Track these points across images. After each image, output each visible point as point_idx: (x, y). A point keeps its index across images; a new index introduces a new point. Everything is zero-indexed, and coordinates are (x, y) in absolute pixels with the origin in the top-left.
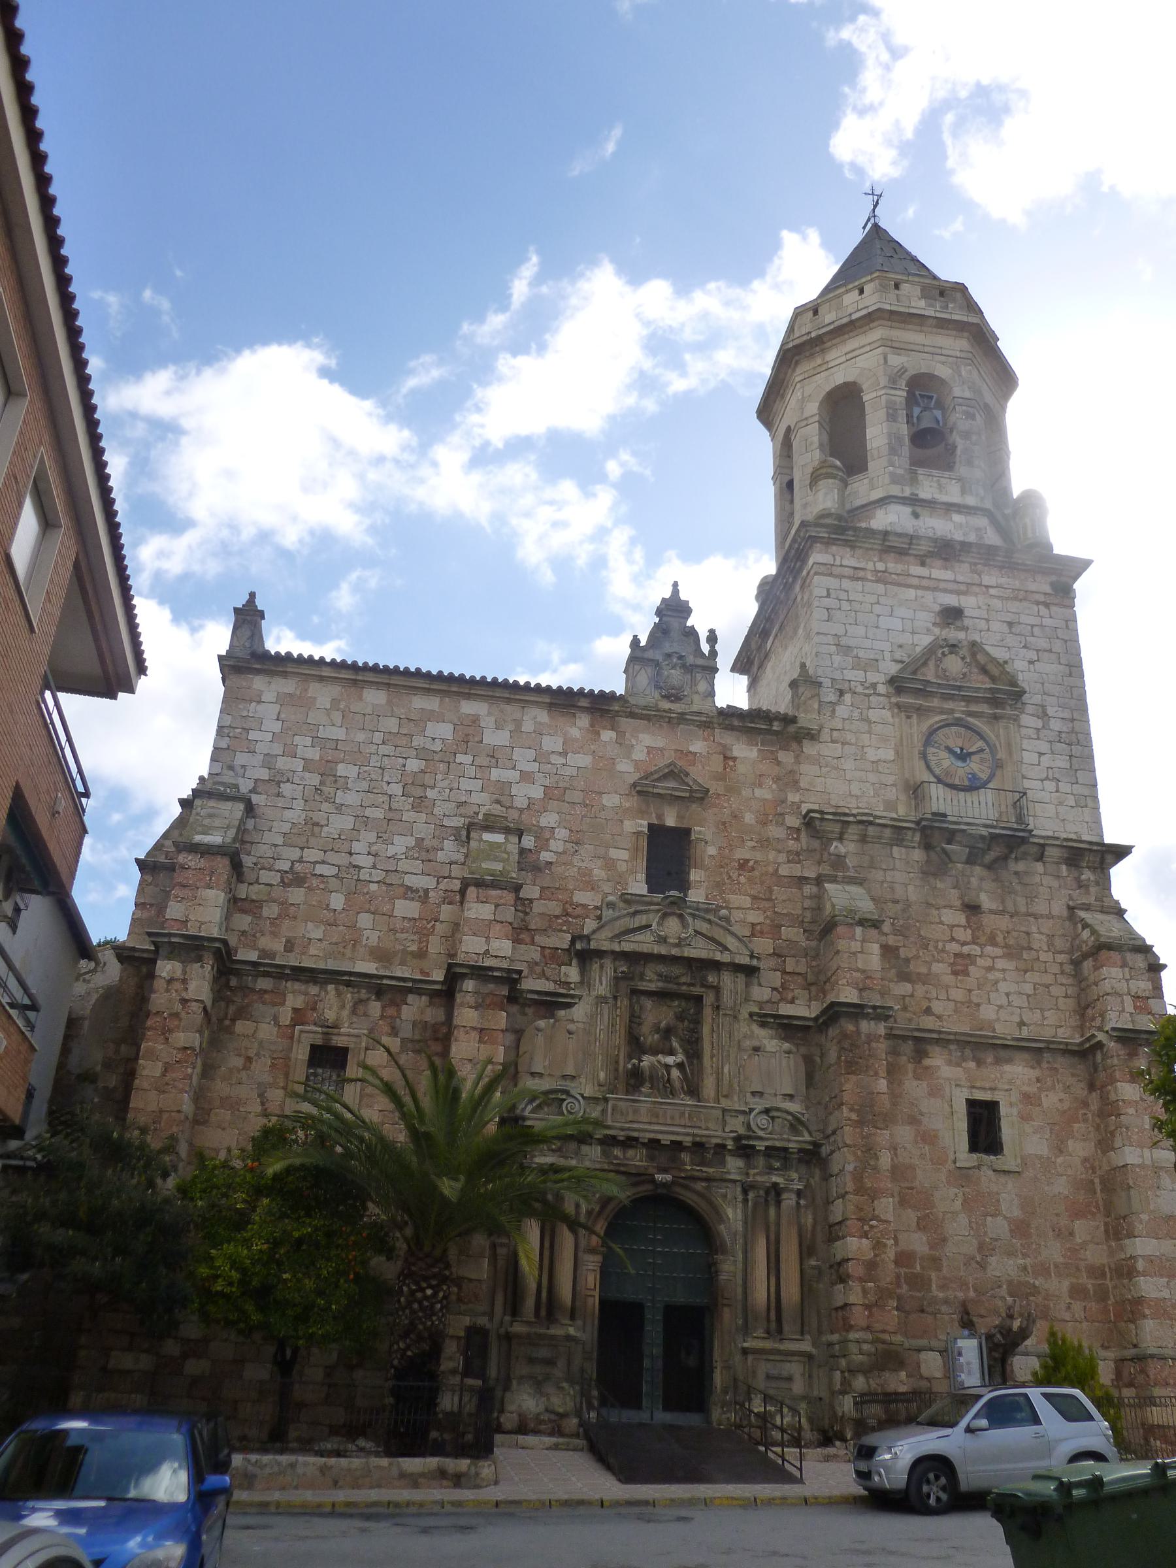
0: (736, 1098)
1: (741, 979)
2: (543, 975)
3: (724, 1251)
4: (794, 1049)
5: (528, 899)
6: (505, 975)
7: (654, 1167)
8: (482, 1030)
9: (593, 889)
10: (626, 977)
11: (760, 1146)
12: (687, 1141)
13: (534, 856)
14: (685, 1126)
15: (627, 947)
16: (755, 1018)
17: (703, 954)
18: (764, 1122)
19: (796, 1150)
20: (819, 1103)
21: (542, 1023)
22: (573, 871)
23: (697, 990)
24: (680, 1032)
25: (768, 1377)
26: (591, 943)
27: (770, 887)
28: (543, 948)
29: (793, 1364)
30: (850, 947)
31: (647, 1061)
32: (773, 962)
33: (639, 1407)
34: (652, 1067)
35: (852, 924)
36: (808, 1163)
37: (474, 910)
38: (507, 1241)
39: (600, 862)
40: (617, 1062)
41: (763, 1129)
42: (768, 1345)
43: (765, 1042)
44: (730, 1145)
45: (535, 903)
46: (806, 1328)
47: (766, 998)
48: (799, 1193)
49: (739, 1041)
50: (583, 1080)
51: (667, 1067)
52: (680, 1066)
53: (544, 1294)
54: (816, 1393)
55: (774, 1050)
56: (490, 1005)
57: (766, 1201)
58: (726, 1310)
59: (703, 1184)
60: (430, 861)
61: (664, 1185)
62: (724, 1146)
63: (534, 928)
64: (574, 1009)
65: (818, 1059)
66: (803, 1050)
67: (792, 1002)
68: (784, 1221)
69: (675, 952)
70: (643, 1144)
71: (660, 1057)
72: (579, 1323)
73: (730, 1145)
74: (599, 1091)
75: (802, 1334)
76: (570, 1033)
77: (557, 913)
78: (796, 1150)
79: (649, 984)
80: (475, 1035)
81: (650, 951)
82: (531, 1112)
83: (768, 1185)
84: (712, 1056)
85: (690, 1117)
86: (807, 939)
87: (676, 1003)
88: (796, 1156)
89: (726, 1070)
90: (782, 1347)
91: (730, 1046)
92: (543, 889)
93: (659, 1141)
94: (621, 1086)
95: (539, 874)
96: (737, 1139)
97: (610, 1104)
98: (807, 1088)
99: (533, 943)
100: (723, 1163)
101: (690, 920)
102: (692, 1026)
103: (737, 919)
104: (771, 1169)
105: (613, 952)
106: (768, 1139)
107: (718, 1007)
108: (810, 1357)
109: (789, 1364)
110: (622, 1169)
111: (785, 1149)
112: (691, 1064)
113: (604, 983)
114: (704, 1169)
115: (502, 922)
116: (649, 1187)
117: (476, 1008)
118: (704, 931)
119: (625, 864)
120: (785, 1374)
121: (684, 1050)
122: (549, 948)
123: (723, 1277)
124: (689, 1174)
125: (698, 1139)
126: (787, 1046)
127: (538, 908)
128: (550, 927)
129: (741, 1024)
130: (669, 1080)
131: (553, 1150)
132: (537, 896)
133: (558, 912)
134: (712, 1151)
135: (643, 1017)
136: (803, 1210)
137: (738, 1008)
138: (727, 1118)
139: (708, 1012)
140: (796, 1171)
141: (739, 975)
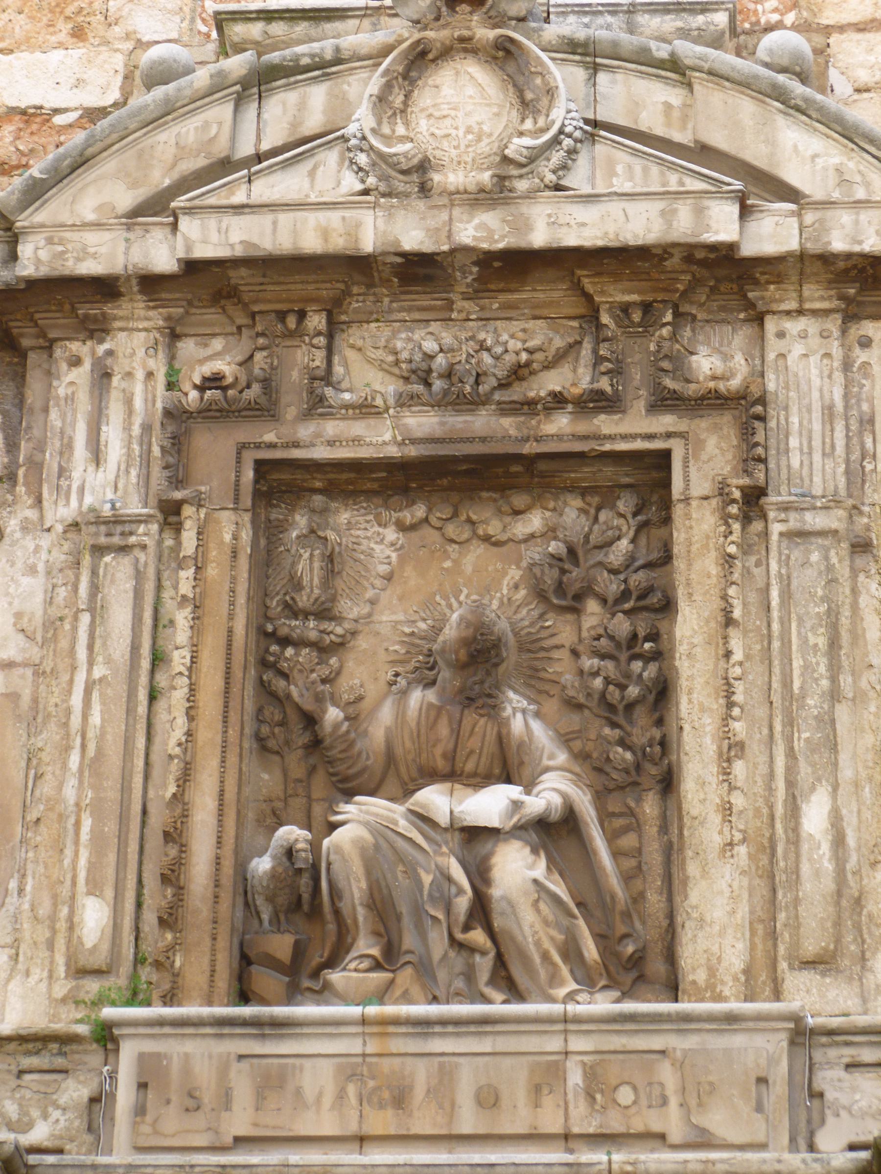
9: (79, 34)
26: (25, 250)
74: (73, 999)
79: (358, 428)
81: (338, 244)
87: (535, 521)
91: (834, 695)
97: (128, 1052)
102: (622, 626)
113: (115, 451)
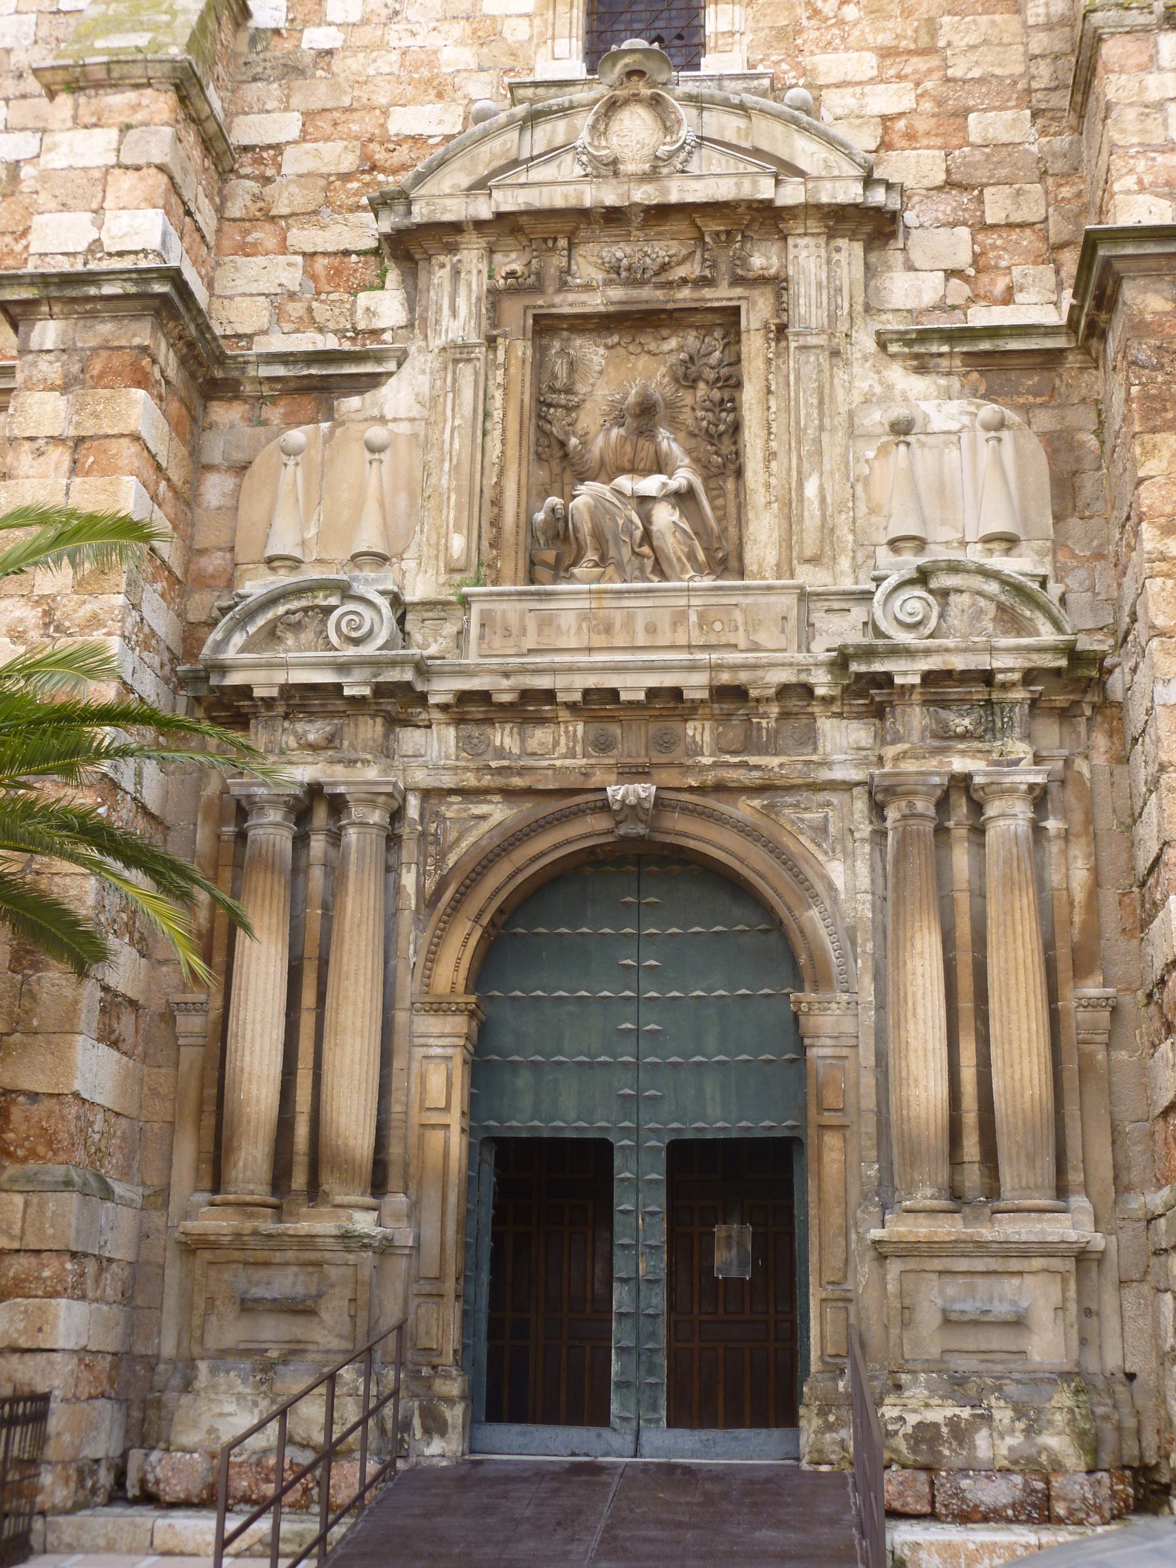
0: (845, 563)
1: (851, 252)
2: (310, 321)
3: (822, 980)
4: (1013, 417)
5: (270, 147)
6: (132, 289)
7: (608, 768)
8: (80, 441)
9: (440, 96)
10: (517, 286)
11: (907, 673)
12: (695, 684)
13: (288, 45)
14: (689, 648)
15: (508, 201)
16: (894, 348)
17: (724, 190)
18: (916, 606)
19: (1016, 676)
20: (1099, 556)
21: (297, 436)
22: (388, 62)
23: (721, 294)
24: (687, 417)
25: (948, 1321)
26: (415, 209)
27: (930, 20)
28: (310, 256)
29: (1028, 1279)
30: (1142, 89)
31: (587, 493)
32: (945, 206)
33: (600, 1418)
34: (599, 508)
35: (1146, 29)
36: (1065, 715)
37: (64, 149)
38: (202, 997)
39: (458, 29)
40: (497, 503)
41: (909, 627)
42: (949, 1228)
43: (928, 407)
44: (822, 682)
45: (289, 153)
46: (1075, 1177)
47: (929, 298)
48: (1039, 798)
49: (851, 415)
50: (409, 565)
51: (644, 501)
52: (683, 498)
53: (302, 1130)
54: (1113, 1360)
55: (955, 426)
56: (101, 376)
57: (941, 831)
58: (832, 1140)
59: (756, 803)
60: (24, 96)
61: (633, 811)
62: (807, 690)
63: (286, 211)
64: (387, 390)
65: (1092, 442)
66: (1045, 420)
67: (1008, 298)
68: (994, 873)
69: (644, 194)
70: (572, 706)
71: (624, 482)
72: (397, 1201)
73: (822, 682)
75: (1062, 1191)
76: (372, 449)
77: (345, 167)
78: (1016, 676)
79: (584, 297)
80: (60, 457)
81: (572, 203)
82: (243, 650)
83: (936, 780)
84: (770, 456)
85: (704, 621)
86: (1043, 132)
87: (673, 343)
88: (1019, 694)
89: (811, 489)
90: (987, 1233)
91: (821, 428)
92: (309, 116)
93: (614, 693)
94: (511, 563)
95: (297, 84)
96: (841, 660)
97: (475, 609)
98: (1058, 518)
99: (283, 249)
100: (810, 738)
101: (687, 114)
102: (716, 395)
103: (839, 112)
104: (945, 737)
105: (479, 225)
106: (927, 652)
107: (782, 329)
108: (1083, 1257)
109: (1015, 1281)
110: (517, 782)
111: (987, 677)
112: (718, 495)
113: (463, 311)
114: (753, 760)
115: (138, 168)
116: (600, 823)
117: (65, 389)
118: (730, 137)
119: (525, 22)
120: (1001, 1309)
121: (696, 460)
122: (324, 254)
123: (820, 1051)
124: (710, 778)
125: (725, 678)
126: (989, 410)
127: (294, 162)
128: (328, 202)
129: (856, 369)
130: (647, 537)
131: (313, 748)
132: (294, 133)
133: (349, 162)
134: (774, 710)
135: (582, 388)
136: (1055, 848)
137: (843, 327)
138: (818, 617)
139: (754, 346)
140: (1028, 737)
141: (843, 243)
